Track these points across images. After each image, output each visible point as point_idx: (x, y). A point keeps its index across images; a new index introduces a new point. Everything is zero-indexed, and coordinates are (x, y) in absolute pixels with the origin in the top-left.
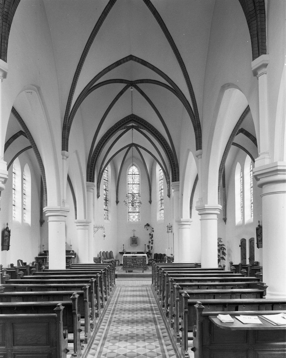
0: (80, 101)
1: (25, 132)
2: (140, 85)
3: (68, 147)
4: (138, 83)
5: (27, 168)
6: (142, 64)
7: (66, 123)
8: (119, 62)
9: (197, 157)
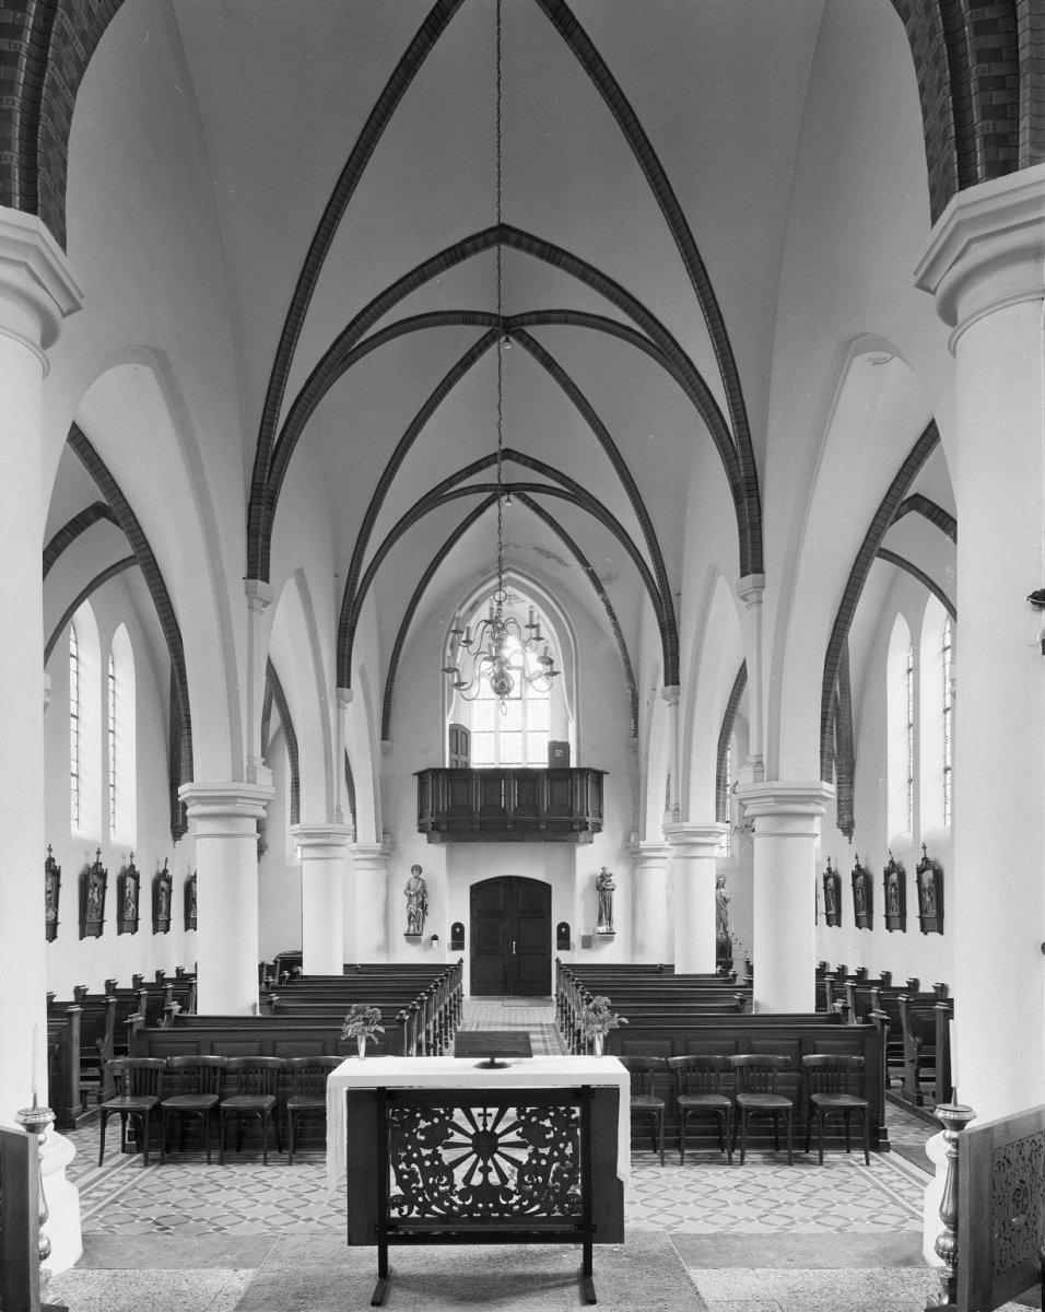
0: (317, 391)
1: (112, 507)
2: (533, 331)
3: (349, 681)
4: (531, 323)
5: (122, 636)
6: (541, 255)
7: (263, 477)
8: (458, 250)
9: (746, 600)
